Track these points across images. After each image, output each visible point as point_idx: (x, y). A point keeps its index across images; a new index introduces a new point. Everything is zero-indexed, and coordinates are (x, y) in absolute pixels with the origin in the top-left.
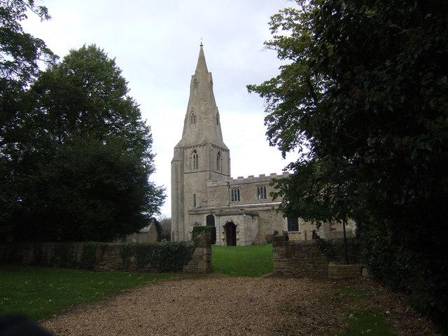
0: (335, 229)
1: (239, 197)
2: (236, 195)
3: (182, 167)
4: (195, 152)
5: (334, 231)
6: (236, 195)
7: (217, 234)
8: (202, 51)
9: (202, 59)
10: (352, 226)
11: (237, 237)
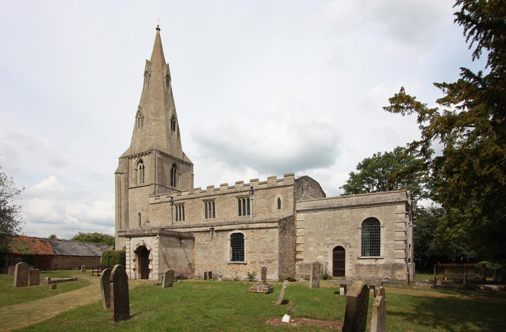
0: (301, 260)
1: (184, 216)
2: (210, 210)
3: (127, 180)
4: (142, 162)
5: (300, 263)
6: (210, 210)
7: (127, 262)
8: (158, 37)
9: (158, 46)
10: (435, 265)
11: (150, 267)
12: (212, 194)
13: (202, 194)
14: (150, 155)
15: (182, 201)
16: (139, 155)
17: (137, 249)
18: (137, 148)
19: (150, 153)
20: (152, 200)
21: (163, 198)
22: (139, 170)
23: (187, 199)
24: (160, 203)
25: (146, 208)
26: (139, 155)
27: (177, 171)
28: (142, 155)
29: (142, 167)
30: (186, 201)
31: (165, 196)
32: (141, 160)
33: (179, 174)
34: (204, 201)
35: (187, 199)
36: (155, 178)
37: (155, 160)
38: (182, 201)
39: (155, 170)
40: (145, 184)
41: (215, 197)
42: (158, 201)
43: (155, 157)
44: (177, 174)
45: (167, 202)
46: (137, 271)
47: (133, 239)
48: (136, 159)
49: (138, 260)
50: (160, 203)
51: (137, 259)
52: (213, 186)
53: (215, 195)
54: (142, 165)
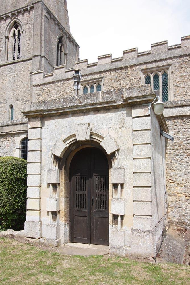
7: (31, 192)
12: (163, 57)
13: (140, 58)
14: (33, 12)
15: (98, 76)
16: (14, 14)
17: (67, 152)
18: (10, 4)
19: (32, 8)
20: (38, 79)
21: (59, 73)
22: (11, 39)
23: (107, 71)
24: (53, 83)
25: (23, 95)
26: (14, 14)
27: (63, 50)
28: (19, 13)
29: (17, 34)
30: (107, 74)
31: (63, 70)
32: (15, 22)
33: (65, 54)
34: (144, 71)
35: (107, 71)
36: (41, 47)
37: (42, 18)
38: (98, 76)
39: (41, 34)
40: (22, 58)
41: (169, 62)
42: (49, 79)
43: (42, 14)
44: (63, 54)
45: (70, 79)
46: (62, 219)
47: (50, 124)
48: (8, 21)
49: (66, 184)
50: (53, 83)
51: (63, 182)
52: (165, 43)
53: (170, 58)
54: (17, 32)
